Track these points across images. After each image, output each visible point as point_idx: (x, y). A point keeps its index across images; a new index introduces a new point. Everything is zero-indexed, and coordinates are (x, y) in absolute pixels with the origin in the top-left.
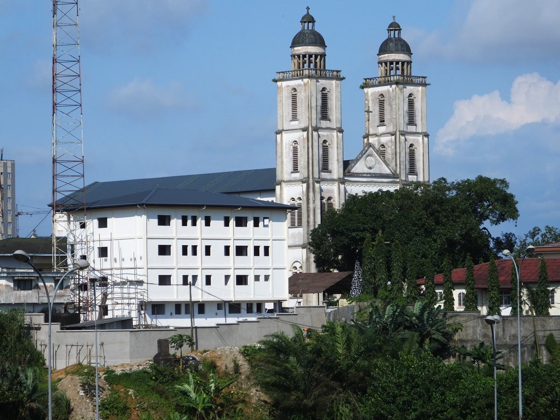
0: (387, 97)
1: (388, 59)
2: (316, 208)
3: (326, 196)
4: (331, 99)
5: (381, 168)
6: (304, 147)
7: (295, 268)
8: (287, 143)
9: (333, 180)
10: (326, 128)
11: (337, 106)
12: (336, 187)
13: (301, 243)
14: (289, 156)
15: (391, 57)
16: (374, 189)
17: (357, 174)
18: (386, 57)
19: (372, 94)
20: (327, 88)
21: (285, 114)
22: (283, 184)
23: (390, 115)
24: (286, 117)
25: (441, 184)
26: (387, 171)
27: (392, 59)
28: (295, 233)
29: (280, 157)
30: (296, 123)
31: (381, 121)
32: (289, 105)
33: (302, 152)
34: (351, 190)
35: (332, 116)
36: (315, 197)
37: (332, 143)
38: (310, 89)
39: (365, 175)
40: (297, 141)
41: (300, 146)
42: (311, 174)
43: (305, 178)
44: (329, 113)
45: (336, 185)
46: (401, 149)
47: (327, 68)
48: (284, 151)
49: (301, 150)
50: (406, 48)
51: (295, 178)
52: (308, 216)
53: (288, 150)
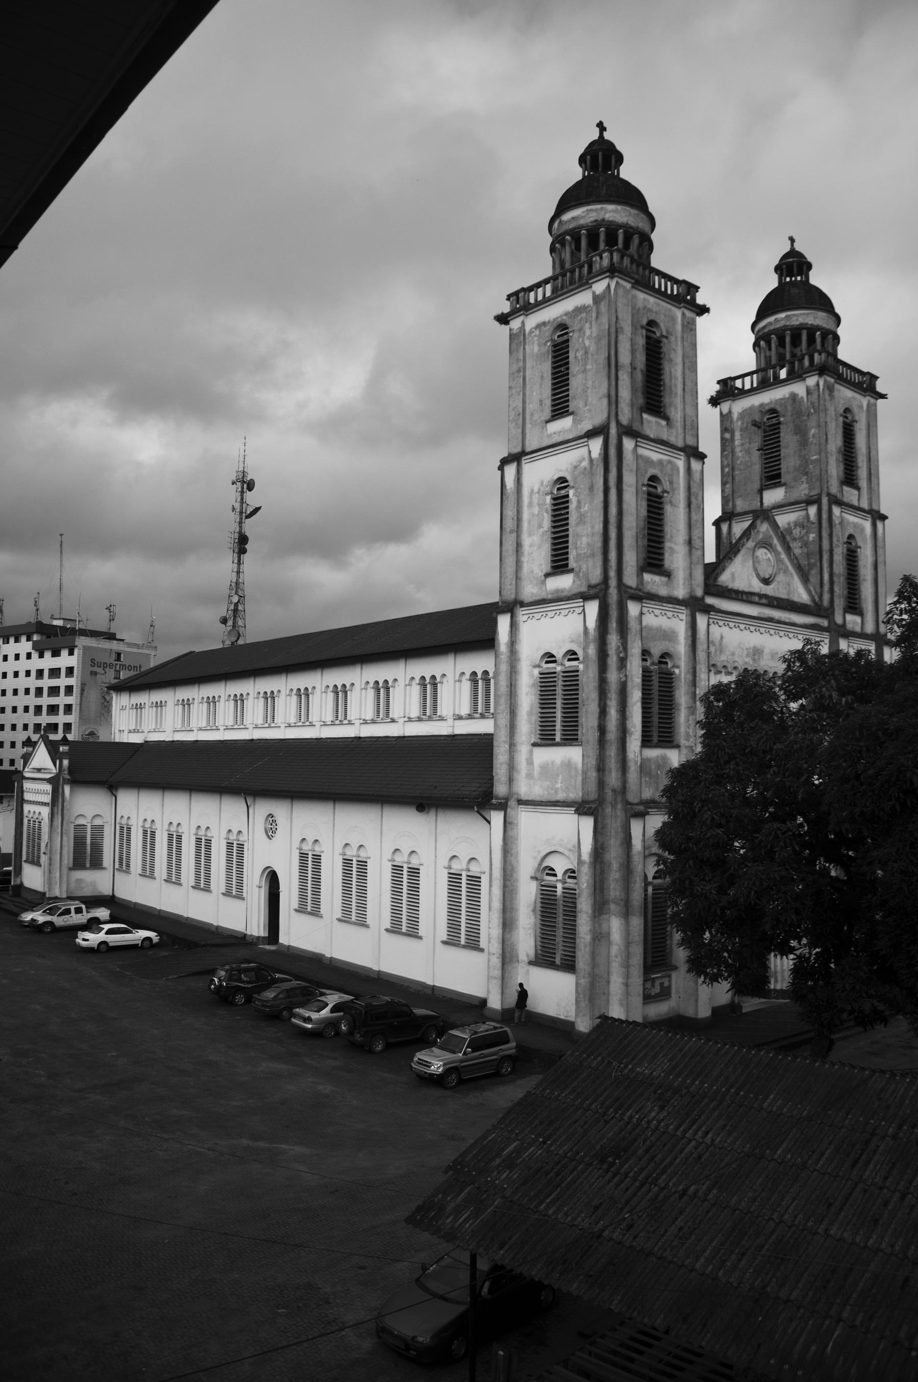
0: (789, 414)
1: (788, 323)
2: (629, 684)
4: (671, 360)
5: (789, 585)
6: (591, 488)
7: (551, 872)
8: (536, 490)
9: (672, 600)
10: (659, 440)
12: (684, 622)
15: (795, 318)
17: (737, 592)
18: (782, 319)
19: (742, 415)
20: (662, 325)
21: (530, 407)
23: (800, 456)
26: (802, 595)
28: (553, 763)
29: (511, 532)
30: (565, 423)
32: (542, 377)
33: (586, 508)
34: (722, 638)
35: (672, 409)
36: (625, 649)
37: (673, 490)
38: (613, 311)
39: (756, 599)
42: (612, 573)
43: (595, 586)
44: (666, 400)
45: (683, 617)
46: (835, 540)
49: (579, 502)
50: (822, 302)
51: (557, 591)
52: (603, 712)
53: (536, 510)
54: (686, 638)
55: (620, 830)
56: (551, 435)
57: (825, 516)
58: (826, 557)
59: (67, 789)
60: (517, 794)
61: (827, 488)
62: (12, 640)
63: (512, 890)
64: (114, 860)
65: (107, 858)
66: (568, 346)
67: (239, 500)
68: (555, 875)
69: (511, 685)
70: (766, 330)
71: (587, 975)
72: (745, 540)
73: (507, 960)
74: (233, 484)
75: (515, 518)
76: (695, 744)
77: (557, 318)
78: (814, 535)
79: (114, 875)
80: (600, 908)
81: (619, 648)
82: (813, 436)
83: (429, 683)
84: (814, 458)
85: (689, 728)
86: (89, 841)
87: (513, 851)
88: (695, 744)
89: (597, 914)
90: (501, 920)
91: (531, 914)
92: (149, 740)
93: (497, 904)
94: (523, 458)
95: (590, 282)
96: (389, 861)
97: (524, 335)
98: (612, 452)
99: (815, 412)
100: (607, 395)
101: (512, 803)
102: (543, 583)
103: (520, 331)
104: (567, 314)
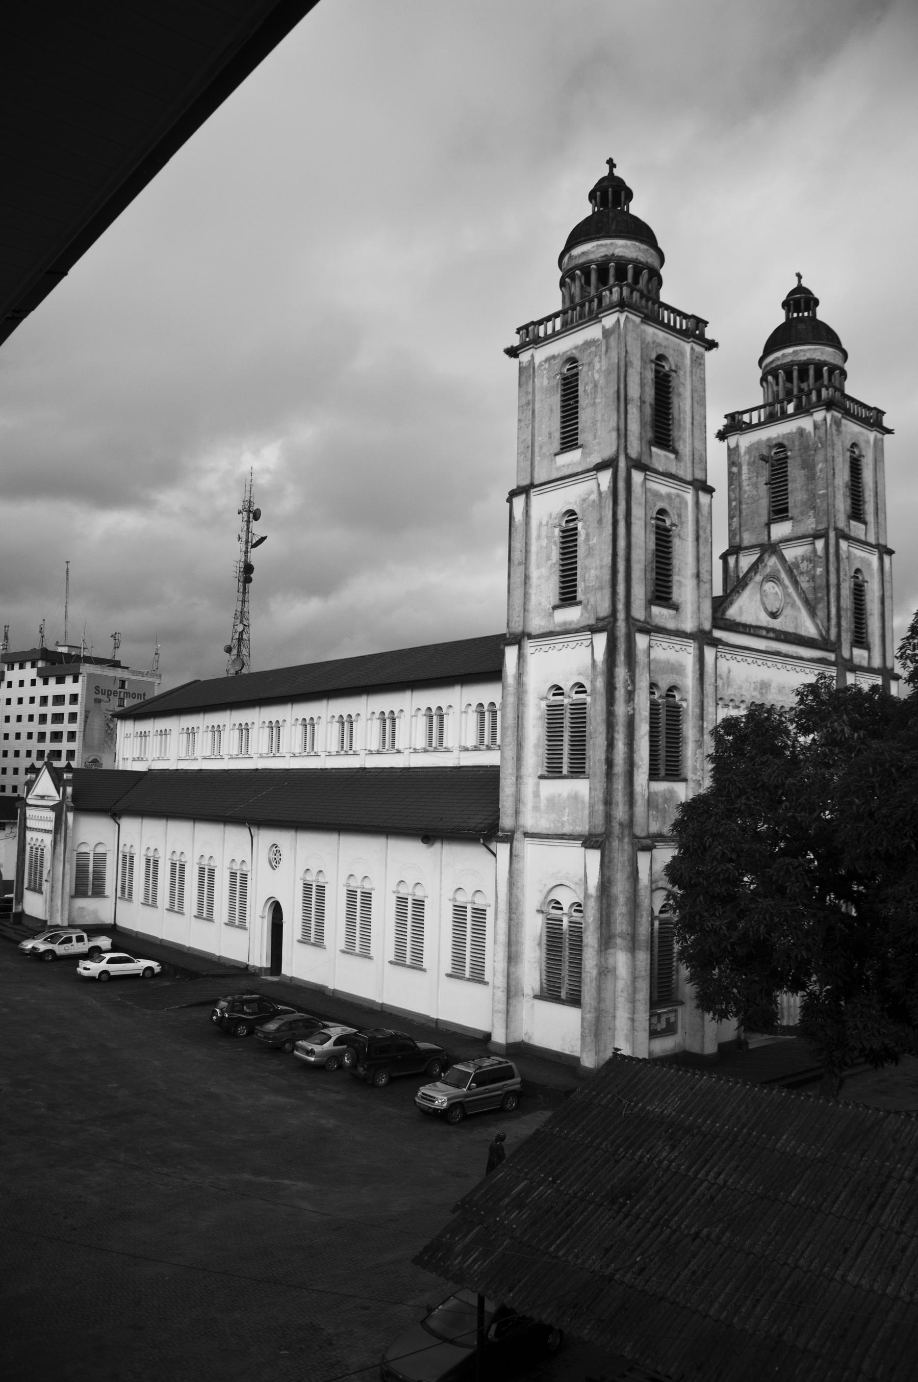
0: (797, 448)
1: (795, 359)
3: (664, 684)
4: (679, 395)
5: (796, 619)
6: (600, 521)
7: (557, 905)
8: (544, 522)
10: (667, 473)
11: (695, 417)
13: (583, 828)
14: (549, 558)
15: (802, 354)
18: (790, 354)
19: (749, 450)
20: (670, 359)
21: (539, 439)
22: (529, 645)
23: (807, 490)
24: (541, 447)
26: (809, 629)
27: (805, 358)
28: (559, 795)
30: (573, 458)
31: (777, 512)
32: (551, 410)
33: (594, 541)
34: (729, 671)
35: (681, 442)
37: (682, 523)
38: (623, 345)
39: (764, 633)
40: (577, 511)
41: (585, 522)
42: (621, 606)
43: (603, 619)
44: (675, 433)
45: (691, 650)
48: (534, 548)
49: (587, 535)
51: (565, 623)
52: (611, 745)
53: (544, 542)
54: (694, 672)
55: (627, 863)
56: (560, 467)
57: (832, 550)
58: (833, 591)
59: (70, 816)
60: (524, 827)
61: (835, 522)
62: (17, 666)
63: (517, 924)
64: (116, 889)
65: (110, 885)
66: (577, 380)
67: (245, 529)
68: (561, 909)
69: (518, 717)
70: (773, 365)
71: (592, 1010)
72: (753, 574)
73: (512, 993)
74: (239, 513)
75: (524, 551)
76: (703, 778)
77: (567, 351)
78: (821, 569)
79: (116, 904)
80: (606, 942)
81: (627, 681)
82: (821, 470)
83: (436, 714)
84: (822, 492)
85: (696, 761)
86: (91, 869)
87: (519, 884)
88: (703, 778)
89: (603, 948)
90: (507, 954)
91: (537, 947)
92: (152, 768)
93: (502, 938)
94: (532, 490)
95: (600, 316)
96: (394, 892)
97: (534, 368)
98: (621, 485)
99: (822, 446)
100: (616, 428)
101: (518, 836)
102: (551, 615)
103: (530, 364)
104: (576, 348)
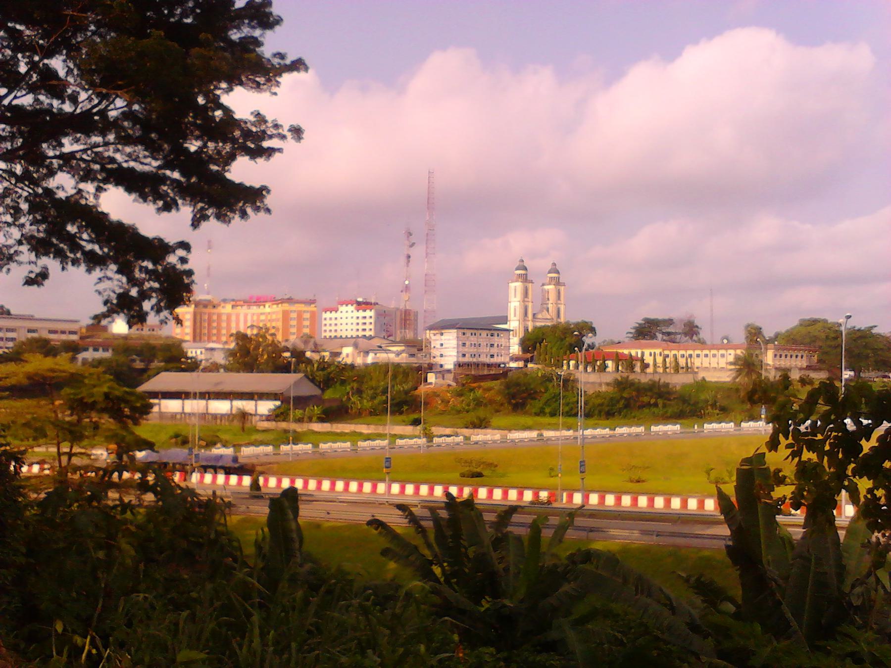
16: (543, 324)
25: (568, 323)
26: (549, 317)
47: (560, 281)
